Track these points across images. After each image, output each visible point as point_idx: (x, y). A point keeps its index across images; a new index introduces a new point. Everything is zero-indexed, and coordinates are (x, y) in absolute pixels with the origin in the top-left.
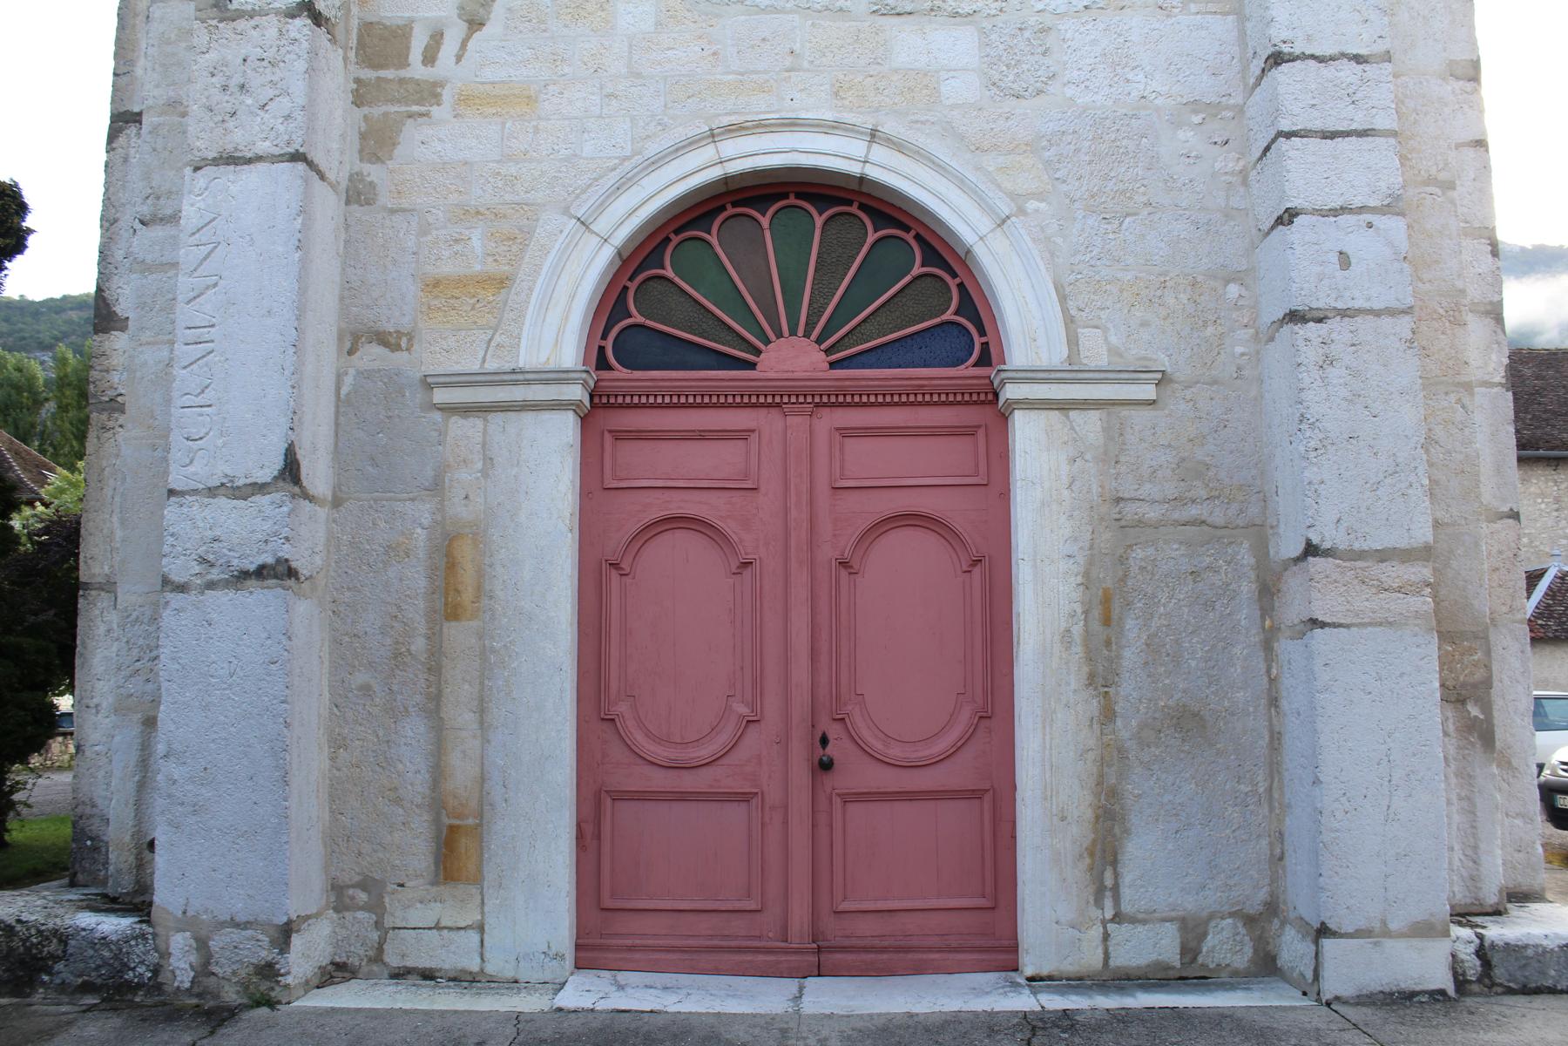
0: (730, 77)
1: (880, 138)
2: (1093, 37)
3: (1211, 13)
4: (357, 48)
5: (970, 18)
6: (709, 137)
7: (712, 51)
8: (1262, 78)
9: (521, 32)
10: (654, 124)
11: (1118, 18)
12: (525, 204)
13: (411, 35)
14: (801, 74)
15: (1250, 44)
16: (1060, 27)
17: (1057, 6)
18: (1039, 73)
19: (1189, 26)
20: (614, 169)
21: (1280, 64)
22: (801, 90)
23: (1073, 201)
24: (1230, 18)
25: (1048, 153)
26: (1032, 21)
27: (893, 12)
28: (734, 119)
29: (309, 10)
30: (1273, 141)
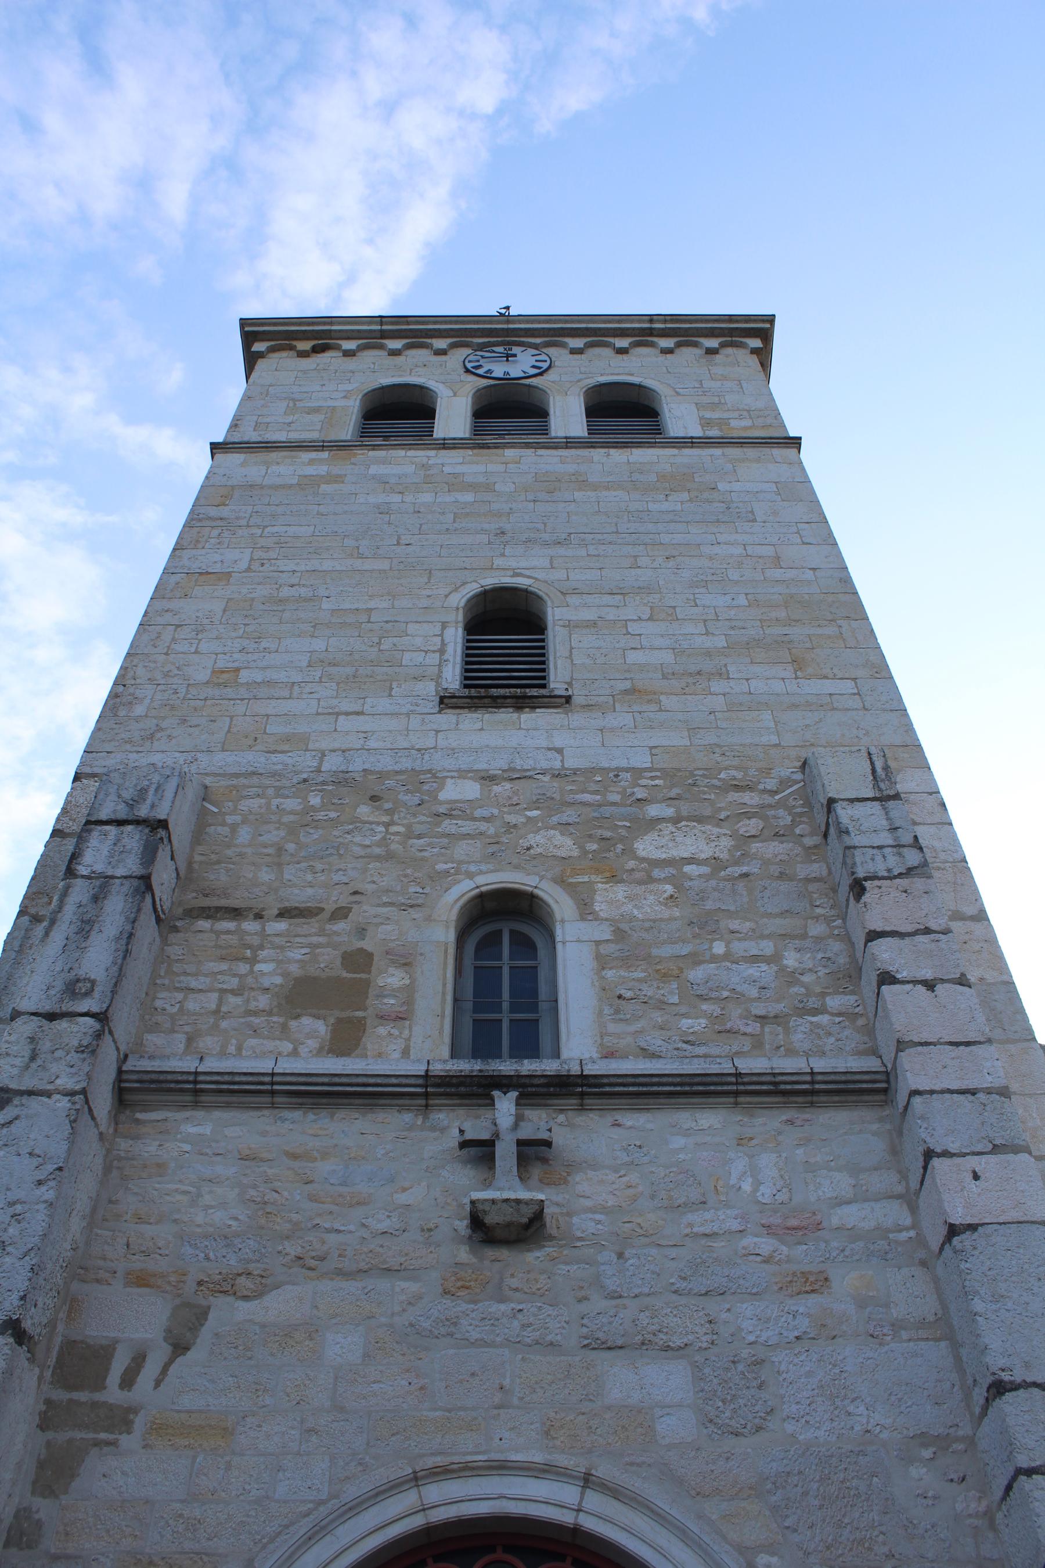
0: (437, 1413)
1: (594, 1483)
2: (808, 1369)
3: (922, 1339)
4: (55, 1368)
5: (681, 1352)
6: (411, 1480)
7: (420, 1385)
8: (987, 1409)
9: (225, 1358)
10: (353, 1464)
11: (831, 1348)
12: (206, 1554)
13: (112, 1356)
14: (510, 1411)
15: (968, 1371)
16: (774, 1359)
17: (768, 1338)
18: (757, 1408)
19: (903, 1354)
20: (307, 1515)
21: (1003, 1394)
22: (511, 1429)
23: (807, 1554)
24: (943, 1344)
25: (774, 1498)
26: (745, 1353)
27: (604, 1346)
28: (439, 1460)
29: (14, 1329)
30: (1014, 1478)
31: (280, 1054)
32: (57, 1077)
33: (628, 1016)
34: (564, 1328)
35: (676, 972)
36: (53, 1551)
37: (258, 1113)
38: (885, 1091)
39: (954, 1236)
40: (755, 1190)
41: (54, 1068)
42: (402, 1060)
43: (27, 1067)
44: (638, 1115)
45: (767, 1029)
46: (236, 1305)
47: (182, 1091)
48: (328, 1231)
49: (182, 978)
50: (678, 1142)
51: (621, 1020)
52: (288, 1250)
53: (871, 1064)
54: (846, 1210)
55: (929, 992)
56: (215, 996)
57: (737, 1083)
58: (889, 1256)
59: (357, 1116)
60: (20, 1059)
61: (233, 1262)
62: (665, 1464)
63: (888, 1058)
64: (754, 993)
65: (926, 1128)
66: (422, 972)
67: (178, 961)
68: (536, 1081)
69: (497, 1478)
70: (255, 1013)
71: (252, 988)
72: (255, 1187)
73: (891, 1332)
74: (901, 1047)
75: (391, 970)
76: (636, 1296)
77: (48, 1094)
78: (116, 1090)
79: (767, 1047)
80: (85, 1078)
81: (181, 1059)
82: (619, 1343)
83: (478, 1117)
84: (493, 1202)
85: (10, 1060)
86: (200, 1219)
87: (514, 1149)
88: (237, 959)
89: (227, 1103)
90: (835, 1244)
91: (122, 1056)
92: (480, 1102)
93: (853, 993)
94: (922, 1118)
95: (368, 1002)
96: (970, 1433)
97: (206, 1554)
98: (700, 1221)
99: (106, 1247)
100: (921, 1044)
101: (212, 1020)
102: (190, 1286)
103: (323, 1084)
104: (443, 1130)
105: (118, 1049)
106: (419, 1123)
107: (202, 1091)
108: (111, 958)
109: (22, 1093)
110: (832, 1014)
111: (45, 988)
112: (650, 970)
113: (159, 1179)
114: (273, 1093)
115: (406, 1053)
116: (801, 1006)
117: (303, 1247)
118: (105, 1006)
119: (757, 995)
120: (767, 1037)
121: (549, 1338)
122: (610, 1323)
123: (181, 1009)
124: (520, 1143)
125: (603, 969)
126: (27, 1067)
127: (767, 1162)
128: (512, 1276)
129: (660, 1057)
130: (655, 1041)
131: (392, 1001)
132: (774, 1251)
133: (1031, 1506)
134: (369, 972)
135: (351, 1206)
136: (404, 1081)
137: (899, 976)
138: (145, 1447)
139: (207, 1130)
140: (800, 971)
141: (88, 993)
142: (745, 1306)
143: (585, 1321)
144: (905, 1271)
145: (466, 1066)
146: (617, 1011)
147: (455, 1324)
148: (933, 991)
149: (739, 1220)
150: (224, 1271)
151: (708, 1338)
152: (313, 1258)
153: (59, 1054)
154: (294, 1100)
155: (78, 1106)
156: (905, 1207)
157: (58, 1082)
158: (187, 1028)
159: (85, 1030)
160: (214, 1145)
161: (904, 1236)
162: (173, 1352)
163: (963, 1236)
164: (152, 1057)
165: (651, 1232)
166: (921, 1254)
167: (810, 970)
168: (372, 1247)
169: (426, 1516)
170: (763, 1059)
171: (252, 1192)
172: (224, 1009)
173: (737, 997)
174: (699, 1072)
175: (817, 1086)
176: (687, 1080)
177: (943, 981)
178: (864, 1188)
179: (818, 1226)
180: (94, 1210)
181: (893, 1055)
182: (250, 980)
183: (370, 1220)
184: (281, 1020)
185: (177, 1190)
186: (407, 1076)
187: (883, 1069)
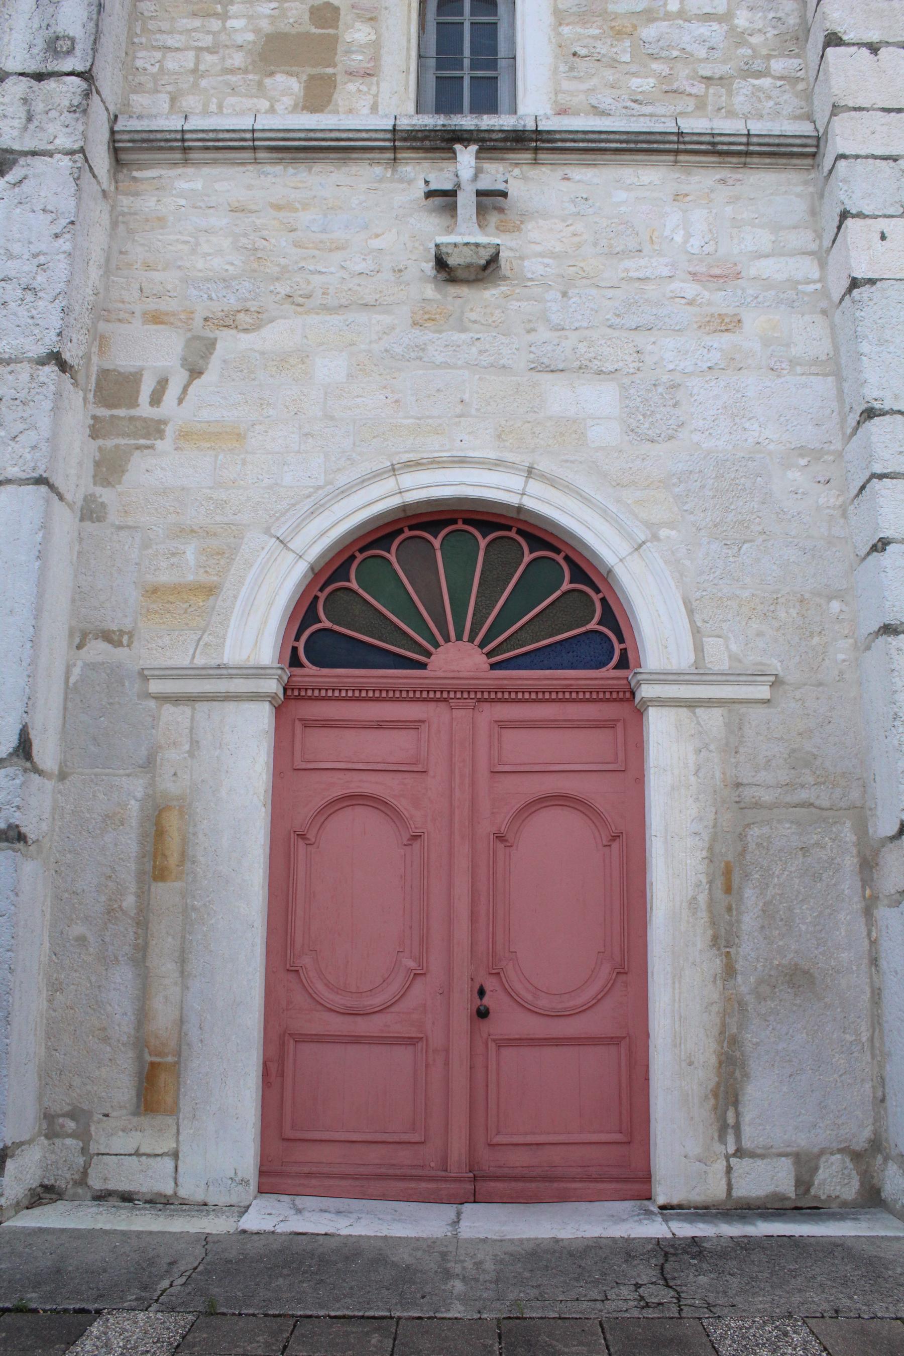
2: (715, 393)
3: (814, 374)
4: (95, 391)
5: (612, 376)
6: (389, 471)
12: (233, 524)
13: (140, 380)
14: (469, 419)
16: (688, 384)
18: (670, 422)
20: (309, 496)
21: (872, 418)
22: (469, 433)
24: (830, 379)
25: (677, 490)
26: (665, 378)
27: (548, 369)
28: (412, 456)
29: (57, 359)
30: (868, 481)
31: (258, 111)
32: (55, 137)
33: (582, 74)
34: (514, 354)
35: (629, 30)
36: (117, 523)
37: (241, 169)
38: (814, 155)
39: (855, 288)
40: (686, 242)
41: (52, 128)
42: (371, 116)
43: (26, 129)
44: (584, 170)
45: (711, 91)
46: (238, 336)
47: (171, 149)
48: (312, 272)
49: (158, 36)
50: (621, 195)
51: (575, 77)
52: (279, 290)
53: (806, 128)
54: (763, 262)
55: (872, 56)
56: (191, 54)
57: (678, 142)
58: (796, 304)
59: (332, 170)
60: (18, 121)
61: (232, 301)
62: (593, 462)
63: (821, 120)
64: (702, 53)
65: (846, 191)
66: (387, 27)
67: (151, 18)
68: (494, 136)
69: (459, 469)
70: (231, 71)
71: (226, 46)
72: (245, 235)
73: (788, 367)
74: (835, 111)
75: (358, 25)
76: (576, 329)
77: (50, 154)
78: (112, 150)
79: (710, 108)
80: (81, 137)
81: (167, 118)
82: (561, 367)
83: (442, 170)
84: (455, 245)
85: (8, 121)
86: (200, 265)
87: (474, 198)
88: (209, 15)
89: (213, 159)
90: (750, 292)
91: (112, 117)
92: (443, 155)
93: (797, 56)
94: (844, 181)
95: (337, 58)
96: (840, 448)
97: (233, 524)
98: (634, 266)
99: (123, 292)
100: (855, 109)
101: (192, 79)
102: (198, 322)
103: (300, 139)
104: (410, 182)
105: (107, 109)
106: (389, 175)
107: (190, 148)
108: (86, 14)
109: (26, 154)
110: (774, 78)
111: (27, 46)
112: (605, 27)
113: (161, 231)
114: (255, 149)
115: (374, 108)
116: (746, 68)
117: (292, 287)
118: (88, 64)
119: (705, 56)
120: (710, 98)
121: (502, 362)
122: (554, 351)
123: (161, 68)
124: (480, 193)
125: (560, 24)
126: (26, 129)
127: (699, 217)
128: (471, 310)
129: (610, 115)
130: (605, 100)
131: (360, 57)
132: (697, 295)
133: (877, 500)
134: (337, 28)
135: (331, 250)
136: (374, 135)
137: (845, 38)
138: (176, 449)
139: (198, 185)
140: (749, 32)
141: (70, 52)
142: (668, 340)
143: (533, 349)
144: (807, 318)
145: (431, 121)
146: (572, 69)
147: (423, 350)
148: (876, 55)
149: (669, 267)
150: (226, 309)
151: (636, 365)
152: (300, 296)
153: (53, 114)
154: (275, 155)
155: (79, 165)
156: (816, 262)
157: (57, 142)
158: (169, 88)
159: (73, 90)
160: (206, 199)
161: (811, 288)
162: (190, 376)
163: (862, 289)
164: (140, 117)
165: (592, 275)
166: (824, 304)
167: (759, 30)
168: (351, 286)
169: (402, 497)
170: (705, 119)
171: (244, 240)
172: (202, 67)
173: (687, 57)
174: (644, 130)
175: (751, 148)
176: (633, 137)
177: (888, 44)
178: (782, 244)
179: (738, 276)
180: (108, 260)
181: (826, 120)
182: (223, 37)
183: (348, 262)
184: (257, 78)
185: (177, 240)
186: (376, 131)
187: (815, 134)
